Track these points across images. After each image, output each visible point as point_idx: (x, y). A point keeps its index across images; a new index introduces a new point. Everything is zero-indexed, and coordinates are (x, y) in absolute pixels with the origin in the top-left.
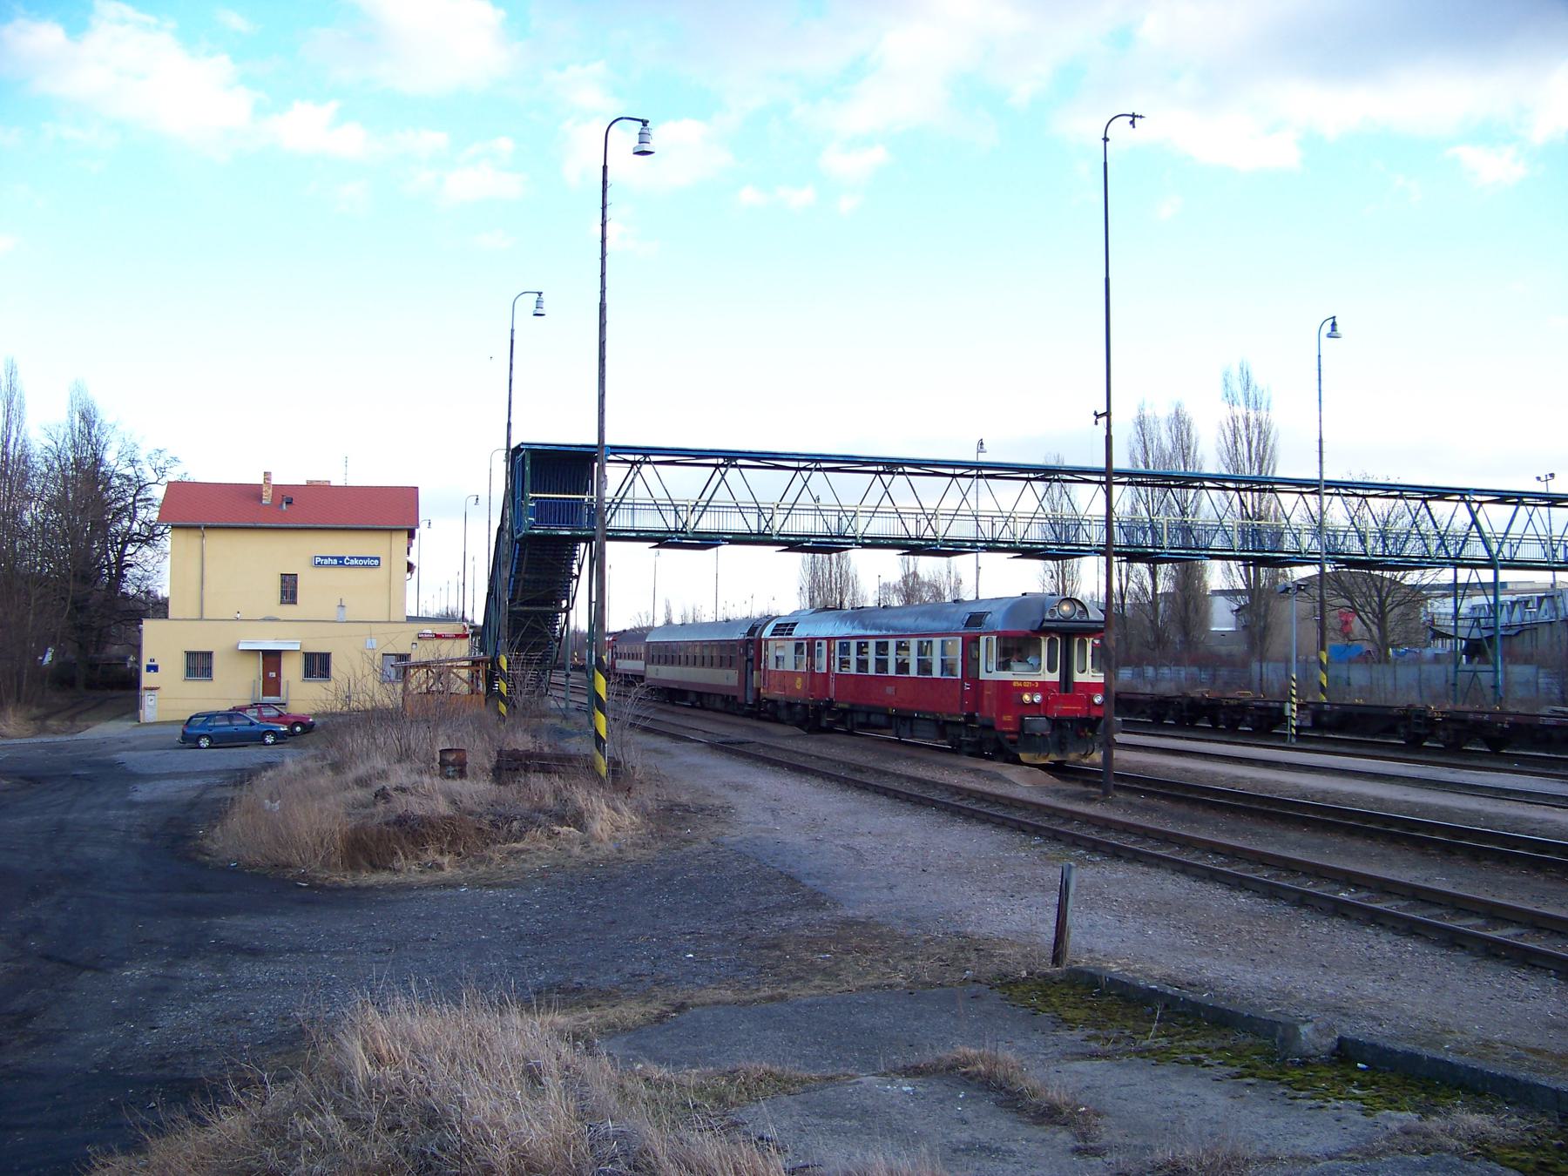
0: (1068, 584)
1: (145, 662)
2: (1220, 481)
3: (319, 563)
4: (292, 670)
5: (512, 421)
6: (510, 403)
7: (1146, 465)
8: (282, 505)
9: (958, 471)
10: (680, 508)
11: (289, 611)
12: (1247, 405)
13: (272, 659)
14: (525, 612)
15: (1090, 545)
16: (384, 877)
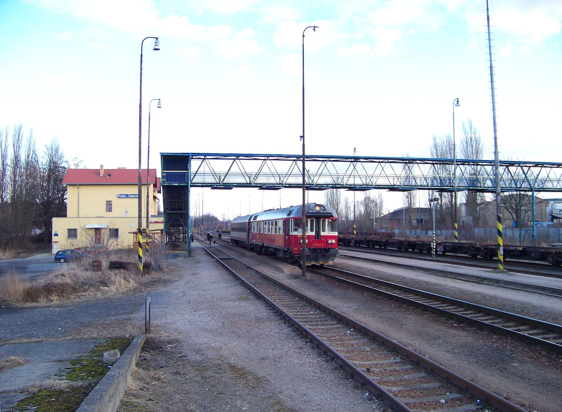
0: (412, 200)
1: (53, 233)
2: (464, 162)
3: (120, 197)
4: (105, 235)
5: (150, 145)
6: (149, 139)
7: (437, 156)
8: (106, 176)
9: (381, 161)
10: (281, 176)
11: (109, 214)
12: (471, 132)
13: (97, 230)
14: (172, 213)
15: (372, 185)
16: (35, 304)
